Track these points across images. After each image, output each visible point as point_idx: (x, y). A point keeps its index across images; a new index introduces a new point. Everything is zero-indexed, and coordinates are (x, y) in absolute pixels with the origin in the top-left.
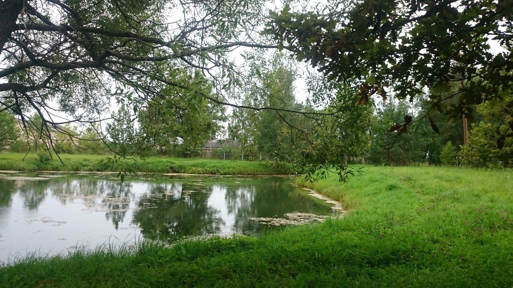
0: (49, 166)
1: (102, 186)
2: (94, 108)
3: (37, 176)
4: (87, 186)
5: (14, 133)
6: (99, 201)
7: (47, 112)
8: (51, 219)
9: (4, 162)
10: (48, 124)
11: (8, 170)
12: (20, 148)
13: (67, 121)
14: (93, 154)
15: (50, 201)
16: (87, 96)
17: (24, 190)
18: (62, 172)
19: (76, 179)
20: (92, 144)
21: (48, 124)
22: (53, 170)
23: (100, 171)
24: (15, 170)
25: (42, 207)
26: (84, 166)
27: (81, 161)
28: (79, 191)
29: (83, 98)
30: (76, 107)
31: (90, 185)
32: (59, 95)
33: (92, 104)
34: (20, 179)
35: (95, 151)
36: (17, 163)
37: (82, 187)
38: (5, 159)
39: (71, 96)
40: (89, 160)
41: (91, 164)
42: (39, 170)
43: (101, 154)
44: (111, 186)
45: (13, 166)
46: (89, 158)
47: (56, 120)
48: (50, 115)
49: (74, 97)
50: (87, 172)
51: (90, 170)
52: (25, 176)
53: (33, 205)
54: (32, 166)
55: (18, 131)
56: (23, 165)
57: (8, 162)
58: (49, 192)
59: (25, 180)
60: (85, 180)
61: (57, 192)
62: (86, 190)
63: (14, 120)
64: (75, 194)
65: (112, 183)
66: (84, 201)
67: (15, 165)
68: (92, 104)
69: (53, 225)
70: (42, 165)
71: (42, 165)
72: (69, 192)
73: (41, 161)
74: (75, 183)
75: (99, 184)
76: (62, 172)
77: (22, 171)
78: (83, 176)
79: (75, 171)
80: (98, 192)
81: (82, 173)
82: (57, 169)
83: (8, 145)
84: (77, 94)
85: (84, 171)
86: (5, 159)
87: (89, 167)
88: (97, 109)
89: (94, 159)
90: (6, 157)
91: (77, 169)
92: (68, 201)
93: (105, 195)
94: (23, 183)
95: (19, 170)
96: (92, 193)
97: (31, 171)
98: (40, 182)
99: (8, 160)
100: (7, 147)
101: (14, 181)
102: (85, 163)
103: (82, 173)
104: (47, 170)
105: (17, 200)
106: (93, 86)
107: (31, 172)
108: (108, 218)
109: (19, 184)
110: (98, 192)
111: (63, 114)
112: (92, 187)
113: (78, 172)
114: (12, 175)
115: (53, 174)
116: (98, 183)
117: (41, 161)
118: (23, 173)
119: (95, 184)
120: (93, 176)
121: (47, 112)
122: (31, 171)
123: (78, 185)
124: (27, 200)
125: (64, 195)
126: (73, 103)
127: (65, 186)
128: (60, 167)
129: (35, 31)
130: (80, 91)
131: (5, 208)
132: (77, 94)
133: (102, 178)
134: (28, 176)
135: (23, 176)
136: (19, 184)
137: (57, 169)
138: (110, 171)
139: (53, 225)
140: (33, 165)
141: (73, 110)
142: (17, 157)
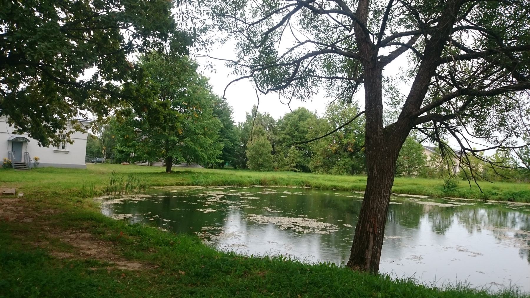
0: (456, 193)
1: (514, 218)
2: (512, 131)
3: (445, 202)
4: (496, 217)
5: (422, 160)
6: (511, 234)
7: (466, 139)
8: (466, 248)
9: (414, 187)
10: (467, 151)
11: (418, 195)
12: (427, 174)
13: (487, 148)
14: (502, 181)
15: (456, 228)
16: (503, 118)
17: (431, 215)
18: (469, 200)
19: (485, 208)
20: (500, 171)
21: (467, 151)
22: (460, 197)
23: (511, 201)
24: (424, 195)
25: (450, 233)
26: (493, 194)
27: (489, 189)
28: (487, 220)
29: (498, 120)
30: (491, 131)
31: (499, 215)
32: (472, 122)
33: (510, 127)
34: (428, 204)
35: (504, 178)
36: (426, 188)
37: (491, 217)
38: (415, 184)
39: (485, 120)
40: (498, 189)
41: (502, 193)
42: (446, 196)
43: (511, 182)
44: (525, 219)
45: (422, 192)
46: (498, 186)
47: (473, 146)
48: (469, 142)
49: (488, 120)
50: (497, 201)
51: (500, 199)
52: (434, 202)
53: (440, 230)
54: (440, 192)
55: (425, 157)
56: (431, 191)
57: (418, 187)
58: (455, 219)
59: (432, 206)
60: (494, 210)
61: (465, 220)
62: (495, 221)
63: (422, 148)
64: (483, 224)
65: (526, 216)
66: (492, 233)
67: (424, 191)
68: (510, 127)
69: (469, 256)
70: (449, 192)
71: (449, 192)
72: (475, 220)
73: (448, 187)
74: (482, 212)
75: (510, 215)
76: (469, 200)
77: (430, 196)
78: (492, 205)
79: (483, 199)
80: (509, 224)
81: (492, 202)
82: (464, 196)
83: (417, 171)
84: (492, 116)
85: (493, 199)
86: (415, 184)
87: (499, 196)
88: (515, 133)
89: (505, 187)
90: (415, 182)
91: (486, 198)
92: (475, 231)
93: (517, 228)
94: (431, 207)
95: (428, 195)
96: (501, 225)
97: (439, 197)
98: (447, 208)
99: (418, 186)
100: (416, 173)
101: (422, 205)
102: (494, 191)
103: (492, 202)
104: (454, 197)
105: (425, 224)
106: (508, 107)
107: (439, 198)
108: (522, 257)
109: (427, 209)
110: (509, 224)
111: (481, 141)
112: (502, 218)
113: (487, 201)
114: (422, 200)
115: (460, 201)
116: (509, 214)
117: (448, 187)
118: (431, 198)
119: (505, 215)
120: (505, 206)
121: (466, 139)
122: (439, 197)
123: (486, 214)
124: (434, 223)
125: (471, 224)
126: (488, 126)
127: (471, 214)
128: (467, 195)
129: (477, 51)
130: (494, 114)
131: (414, 229)
132: (492, 116)
133: (514, 209)
134: (436, 202)
135: (431, 201)
136: (427, 209)
137: (464, 196)
138: (525, 202)
139: (469, 256)
140: (441, 191)
141: (487, 135)
142: (425, 183)
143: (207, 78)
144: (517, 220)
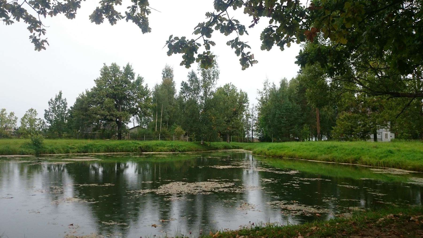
26: (71, 148)
85: (73, 153)
87: (76, 150)
143: (102, 66)
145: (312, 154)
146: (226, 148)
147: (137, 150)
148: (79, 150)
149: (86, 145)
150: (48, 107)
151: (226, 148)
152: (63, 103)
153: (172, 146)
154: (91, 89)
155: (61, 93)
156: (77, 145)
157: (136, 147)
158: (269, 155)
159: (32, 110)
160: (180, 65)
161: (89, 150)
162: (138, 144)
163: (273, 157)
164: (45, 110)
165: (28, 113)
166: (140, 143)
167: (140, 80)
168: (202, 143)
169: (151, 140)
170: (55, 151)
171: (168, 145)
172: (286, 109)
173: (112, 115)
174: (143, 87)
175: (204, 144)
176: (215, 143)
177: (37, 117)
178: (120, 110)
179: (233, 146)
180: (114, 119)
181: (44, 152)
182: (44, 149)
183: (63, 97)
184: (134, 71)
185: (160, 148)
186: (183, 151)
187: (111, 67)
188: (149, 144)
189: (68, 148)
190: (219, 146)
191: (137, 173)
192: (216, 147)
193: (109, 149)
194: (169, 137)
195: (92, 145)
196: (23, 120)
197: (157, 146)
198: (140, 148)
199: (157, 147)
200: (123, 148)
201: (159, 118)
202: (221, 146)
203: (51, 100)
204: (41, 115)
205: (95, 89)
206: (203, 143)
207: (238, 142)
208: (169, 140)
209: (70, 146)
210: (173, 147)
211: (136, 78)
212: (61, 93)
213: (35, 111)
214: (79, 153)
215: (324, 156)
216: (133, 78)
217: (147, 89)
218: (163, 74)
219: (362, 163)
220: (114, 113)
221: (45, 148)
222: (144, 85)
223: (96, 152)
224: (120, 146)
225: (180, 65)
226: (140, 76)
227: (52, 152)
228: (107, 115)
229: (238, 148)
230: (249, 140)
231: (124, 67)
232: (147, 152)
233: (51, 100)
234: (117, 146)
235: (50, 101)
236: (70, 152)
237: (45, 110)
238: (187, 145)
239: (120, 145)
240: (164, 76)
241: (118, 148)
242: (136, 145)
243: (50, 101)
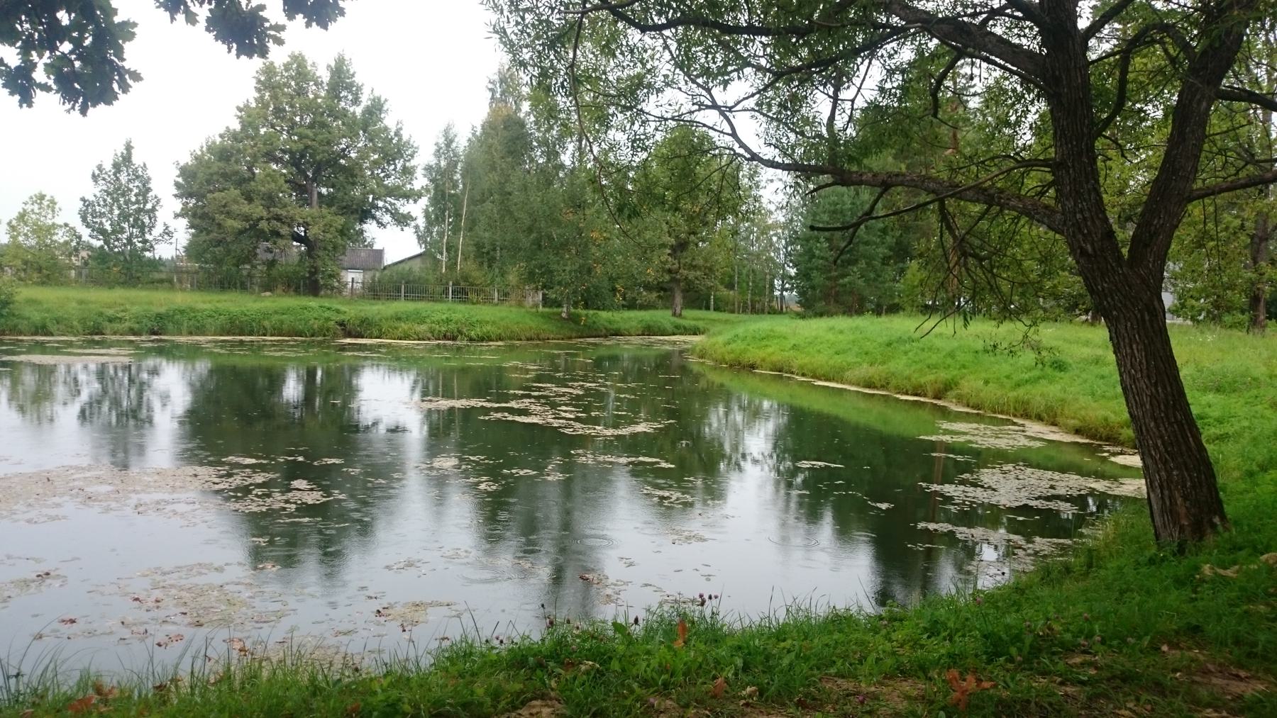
26: (110, 321)
85: (115, 333)
87: (127, 324)
110: (60, 391)
144: (82, 377)
145: (838, 360)
146: (649, 330)
147: (328, 330)
148: (137, 326)
149: (162, 310)
150: (92, 191)
151: (649, 330)
152: (138, 177)
153: (448, 321)
154: (221, 136)
155: (129, 148)
156: (135, 309)
157: (328, 319)
158: (723, 361)
159: (42, 197)
160: (141, 79)
161: (170, 326)
162: (338, 311)
163: (731, 366)
164: (83, 200)
165: (29, 208)
166: (343, 308)
167: (376, 109)
168: (564, 315)
169: (421, 299)
170: (53, 328)
171: (437, 317)
172: (834, 212)
173: (278, 218)
174: (386, 129)
175: (573, 319)
176: (604, 315)
177: (59, 220)
178: (315, 203)
179: (677, 327)
180: (284, 230)
181: (15, 330)
182: (16, 321)
183: (137, 159)
184: (358, 79)
185: (404, 326)
186: (482, 340)
187: (287, 67)
188: (369, 315)
189: (100, 320)
190: (623, 326)
191: (417, 396)
192: (615, 326)
193: (236, 326)
194: (478, 293)
195: (182, 312)
196: (84, 219)
197: (399, 319)
198: (342, 324)
199: (397, 324)
200: (282, 322)
201: (456, 230)
202: (634, 324)
203: (100, 168)
204: (69, 215)
205: (235, 136)
206: (569, 314)
207: (732, 312)
208: (478, 303)
209: (110, 312)
210: (452, 326)
211: (365, 100)
212: (129, 148)
213: (53, 202)
214: (134, 334)
215: (865, 370)
216: (356, 101)
217: (400, 139)
218: (490, 90)
219: (960, 399)
220: (284, 213)
221: (20, 317)
222: (389, 121)
223: (191, 334)
224: (277, 317)
225: (141, 79)
226: (377, 94)
227: (43, 330)
228: (262, 218)
229: (696, 331)
230: (770, 307)
231: (329, 66)
232: (362, 337)
233: (100, 168)
234: (266, 315)
235: (97, 172)
236: (108, 331)
237: (83, 200)
238: (502, 319)
239: (276, 312)
240: (493, 98)
241: (266, 323)
242: (326, 314)
243: (97, 172)
